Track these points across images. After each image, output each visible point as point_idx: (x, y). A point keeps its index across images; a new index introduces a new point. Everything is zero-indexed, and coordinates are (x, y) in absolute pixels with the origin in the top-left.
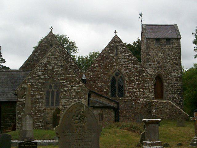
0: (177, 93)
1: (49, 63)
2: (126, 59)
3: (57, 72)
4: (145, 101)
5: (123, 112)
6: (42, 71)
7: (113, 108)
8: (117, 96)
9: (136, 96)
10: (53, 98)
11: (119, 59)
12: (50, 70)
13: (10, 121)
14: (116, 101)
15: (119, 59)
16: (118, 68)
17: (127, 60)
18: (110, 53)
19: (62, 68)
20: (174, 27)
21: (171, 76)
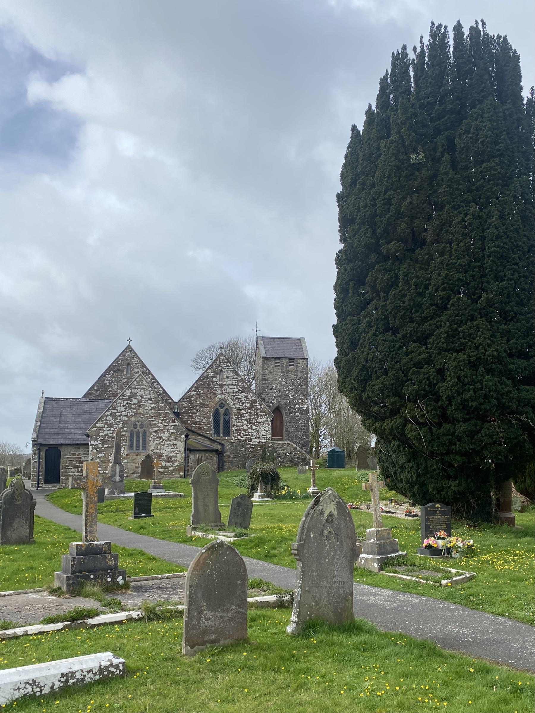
0: (302, 431)
1: (133, 395)
2: (234, 385)
3: (144, 408)
4: (260, 442)
5: (229, 457)
6: (124, 406)
7: (216, 451)
8: (222, 435)
9: (246, 435)
10: (138, 440)
11: (225, 385)
12: (135, 404)
13: (73, 470)
14: (220, 441)
15: (225, 385)
16: (223, 397)
17: (235, 387)
18: (213, 377)
19: (151, 402)
20: (298, 342)
21: (294, 409)
